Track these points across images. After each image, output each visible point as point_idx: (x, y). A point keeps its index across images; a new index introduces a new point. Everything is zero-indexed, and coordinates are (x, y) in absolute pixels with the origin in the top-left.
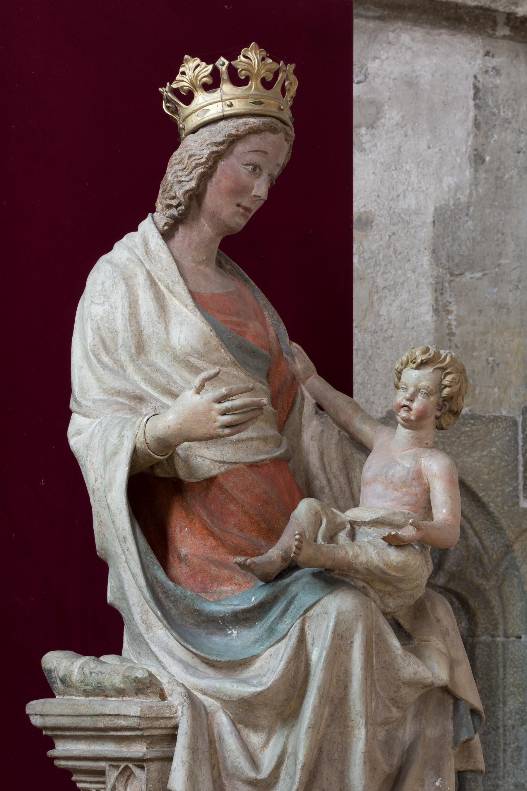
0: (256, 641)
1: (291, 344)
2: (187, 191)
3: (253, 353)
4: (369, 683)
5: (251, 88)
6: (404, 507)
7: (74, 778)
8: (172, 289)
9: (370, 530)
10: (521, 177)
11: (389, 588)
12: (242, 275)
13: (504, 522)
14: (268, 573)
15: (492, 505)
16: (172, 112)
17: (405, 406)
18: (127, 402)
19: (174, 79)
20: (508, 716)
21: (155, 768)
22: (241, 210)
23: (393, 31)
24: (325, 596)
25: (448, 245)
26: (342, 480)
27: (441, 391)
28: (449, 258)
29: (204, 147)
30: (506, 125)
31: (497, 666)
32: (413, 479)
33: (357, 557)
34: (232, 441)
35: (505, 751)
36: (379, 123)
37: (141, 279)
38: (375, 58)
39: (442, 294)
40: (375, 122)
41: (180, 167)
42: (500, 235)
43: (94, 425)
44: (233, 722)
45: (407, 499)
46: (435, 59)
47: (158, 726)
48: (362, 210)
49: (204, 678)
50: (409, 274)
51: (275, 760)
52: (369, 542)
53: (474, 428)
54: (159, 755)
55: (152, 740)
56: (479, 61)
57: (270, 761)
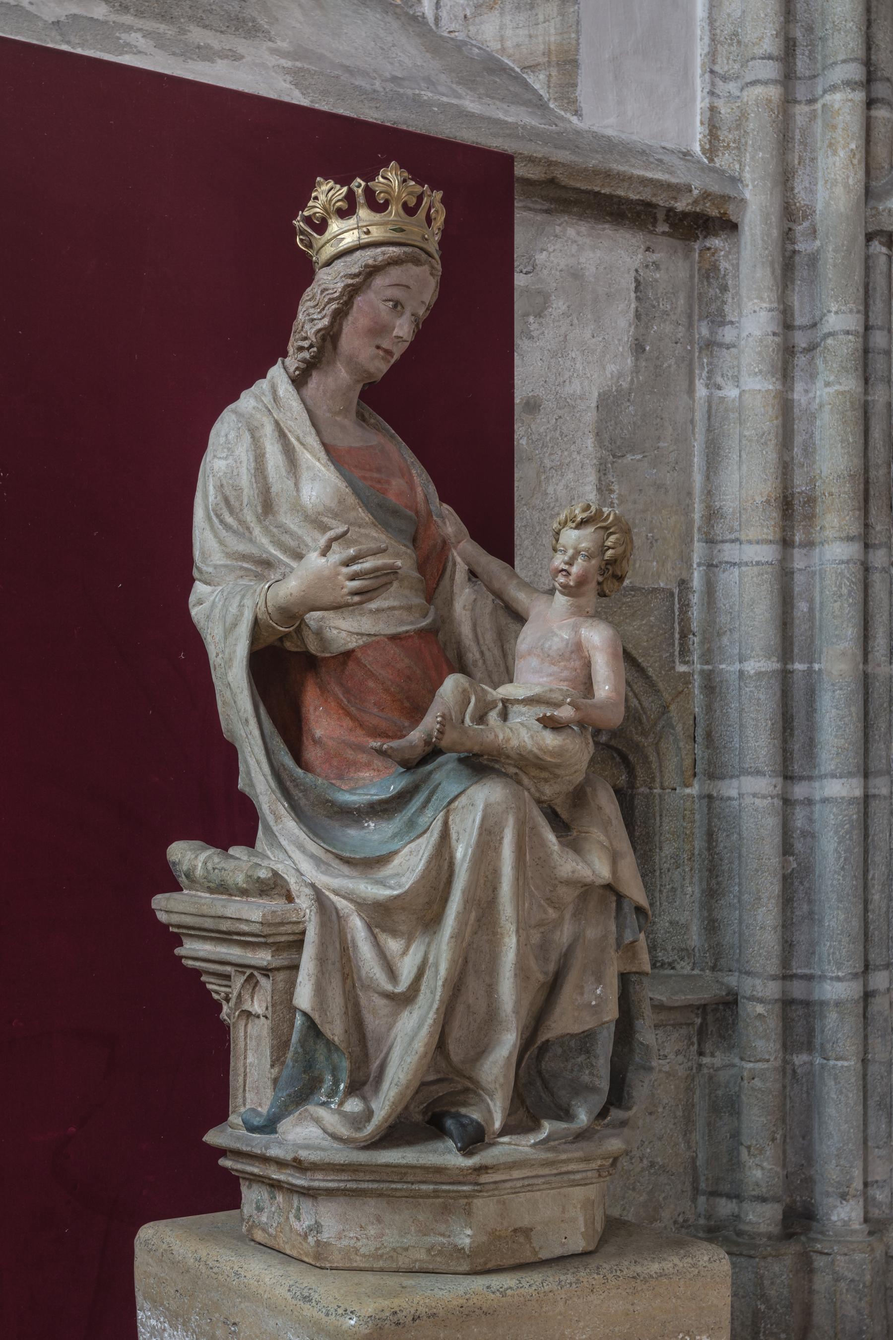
0: (394, 836)
1: (441, 505)
2: (319, 330)
3: (395, 513)
4: (521, 883)
5: (391, 212)
6: (562, 683)
7: (203, 978)
8: (303, 441)
9: (524, 709)
10: (678, 366)
11: (544, 775)
12: (387, 431)
13: (661, 685)
14: (409, 759)
15: (650, 669)
16: (306, 246)
17: (563, 570)
18: (253, 568)
19: (306, 206)
20: (664, 860)
21: (282, 977)
22: (381, 353)
23: (559, 225)
24: (471, 785)
25: (611, 428)
26: (497, 652)
27: (604, 553)
28: (612, 441)
29: (338, 280)
30: (665, 317)
31: (654, 815)
32: (572, 652)
33: (508, 740)
34: (371, 611)
35: (661, 891)
36: (546, 312)
37: (268, 429)
38: (542, 250)
39: (605, 474)
40: (542, 311)
41: (311, 304)
42: (659, 420)
43: (216, 593)
44: (369, 927)
45: (566, 674)
46: (598, 253)
47: (283, 932)
48: (530, 395)
49: (337, 876)
50: (575, 455)
51: (415, 970)
52: (522, 724)
53: (634, 599)
54: (286, 963)
55: (278, 948)
56: (640, 256)
57: (409, 972)
